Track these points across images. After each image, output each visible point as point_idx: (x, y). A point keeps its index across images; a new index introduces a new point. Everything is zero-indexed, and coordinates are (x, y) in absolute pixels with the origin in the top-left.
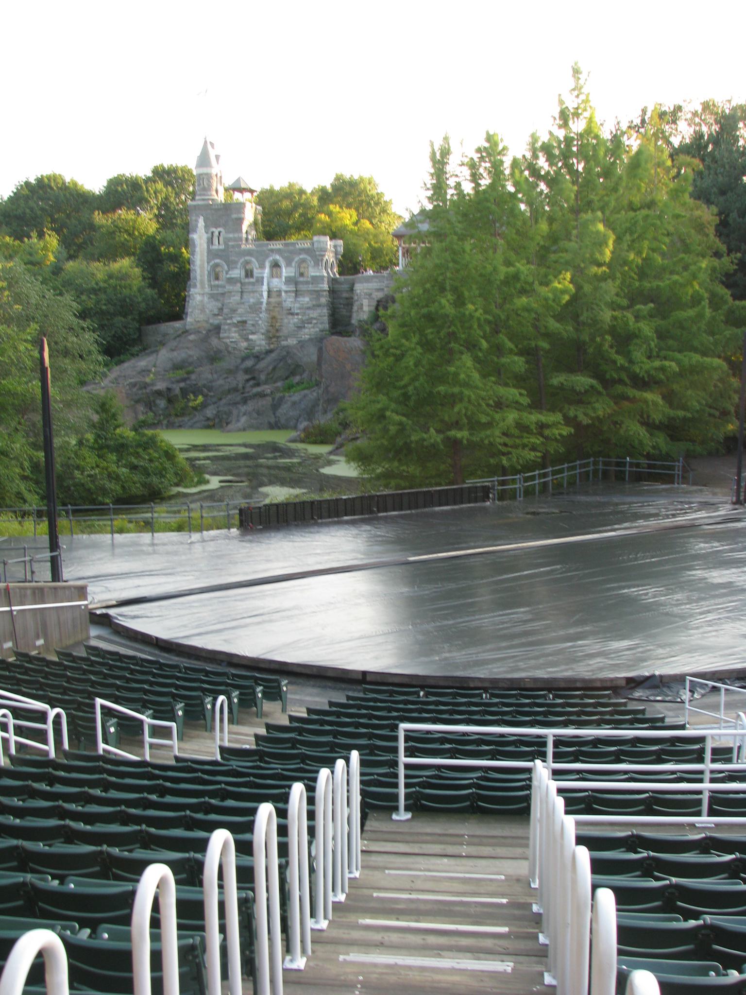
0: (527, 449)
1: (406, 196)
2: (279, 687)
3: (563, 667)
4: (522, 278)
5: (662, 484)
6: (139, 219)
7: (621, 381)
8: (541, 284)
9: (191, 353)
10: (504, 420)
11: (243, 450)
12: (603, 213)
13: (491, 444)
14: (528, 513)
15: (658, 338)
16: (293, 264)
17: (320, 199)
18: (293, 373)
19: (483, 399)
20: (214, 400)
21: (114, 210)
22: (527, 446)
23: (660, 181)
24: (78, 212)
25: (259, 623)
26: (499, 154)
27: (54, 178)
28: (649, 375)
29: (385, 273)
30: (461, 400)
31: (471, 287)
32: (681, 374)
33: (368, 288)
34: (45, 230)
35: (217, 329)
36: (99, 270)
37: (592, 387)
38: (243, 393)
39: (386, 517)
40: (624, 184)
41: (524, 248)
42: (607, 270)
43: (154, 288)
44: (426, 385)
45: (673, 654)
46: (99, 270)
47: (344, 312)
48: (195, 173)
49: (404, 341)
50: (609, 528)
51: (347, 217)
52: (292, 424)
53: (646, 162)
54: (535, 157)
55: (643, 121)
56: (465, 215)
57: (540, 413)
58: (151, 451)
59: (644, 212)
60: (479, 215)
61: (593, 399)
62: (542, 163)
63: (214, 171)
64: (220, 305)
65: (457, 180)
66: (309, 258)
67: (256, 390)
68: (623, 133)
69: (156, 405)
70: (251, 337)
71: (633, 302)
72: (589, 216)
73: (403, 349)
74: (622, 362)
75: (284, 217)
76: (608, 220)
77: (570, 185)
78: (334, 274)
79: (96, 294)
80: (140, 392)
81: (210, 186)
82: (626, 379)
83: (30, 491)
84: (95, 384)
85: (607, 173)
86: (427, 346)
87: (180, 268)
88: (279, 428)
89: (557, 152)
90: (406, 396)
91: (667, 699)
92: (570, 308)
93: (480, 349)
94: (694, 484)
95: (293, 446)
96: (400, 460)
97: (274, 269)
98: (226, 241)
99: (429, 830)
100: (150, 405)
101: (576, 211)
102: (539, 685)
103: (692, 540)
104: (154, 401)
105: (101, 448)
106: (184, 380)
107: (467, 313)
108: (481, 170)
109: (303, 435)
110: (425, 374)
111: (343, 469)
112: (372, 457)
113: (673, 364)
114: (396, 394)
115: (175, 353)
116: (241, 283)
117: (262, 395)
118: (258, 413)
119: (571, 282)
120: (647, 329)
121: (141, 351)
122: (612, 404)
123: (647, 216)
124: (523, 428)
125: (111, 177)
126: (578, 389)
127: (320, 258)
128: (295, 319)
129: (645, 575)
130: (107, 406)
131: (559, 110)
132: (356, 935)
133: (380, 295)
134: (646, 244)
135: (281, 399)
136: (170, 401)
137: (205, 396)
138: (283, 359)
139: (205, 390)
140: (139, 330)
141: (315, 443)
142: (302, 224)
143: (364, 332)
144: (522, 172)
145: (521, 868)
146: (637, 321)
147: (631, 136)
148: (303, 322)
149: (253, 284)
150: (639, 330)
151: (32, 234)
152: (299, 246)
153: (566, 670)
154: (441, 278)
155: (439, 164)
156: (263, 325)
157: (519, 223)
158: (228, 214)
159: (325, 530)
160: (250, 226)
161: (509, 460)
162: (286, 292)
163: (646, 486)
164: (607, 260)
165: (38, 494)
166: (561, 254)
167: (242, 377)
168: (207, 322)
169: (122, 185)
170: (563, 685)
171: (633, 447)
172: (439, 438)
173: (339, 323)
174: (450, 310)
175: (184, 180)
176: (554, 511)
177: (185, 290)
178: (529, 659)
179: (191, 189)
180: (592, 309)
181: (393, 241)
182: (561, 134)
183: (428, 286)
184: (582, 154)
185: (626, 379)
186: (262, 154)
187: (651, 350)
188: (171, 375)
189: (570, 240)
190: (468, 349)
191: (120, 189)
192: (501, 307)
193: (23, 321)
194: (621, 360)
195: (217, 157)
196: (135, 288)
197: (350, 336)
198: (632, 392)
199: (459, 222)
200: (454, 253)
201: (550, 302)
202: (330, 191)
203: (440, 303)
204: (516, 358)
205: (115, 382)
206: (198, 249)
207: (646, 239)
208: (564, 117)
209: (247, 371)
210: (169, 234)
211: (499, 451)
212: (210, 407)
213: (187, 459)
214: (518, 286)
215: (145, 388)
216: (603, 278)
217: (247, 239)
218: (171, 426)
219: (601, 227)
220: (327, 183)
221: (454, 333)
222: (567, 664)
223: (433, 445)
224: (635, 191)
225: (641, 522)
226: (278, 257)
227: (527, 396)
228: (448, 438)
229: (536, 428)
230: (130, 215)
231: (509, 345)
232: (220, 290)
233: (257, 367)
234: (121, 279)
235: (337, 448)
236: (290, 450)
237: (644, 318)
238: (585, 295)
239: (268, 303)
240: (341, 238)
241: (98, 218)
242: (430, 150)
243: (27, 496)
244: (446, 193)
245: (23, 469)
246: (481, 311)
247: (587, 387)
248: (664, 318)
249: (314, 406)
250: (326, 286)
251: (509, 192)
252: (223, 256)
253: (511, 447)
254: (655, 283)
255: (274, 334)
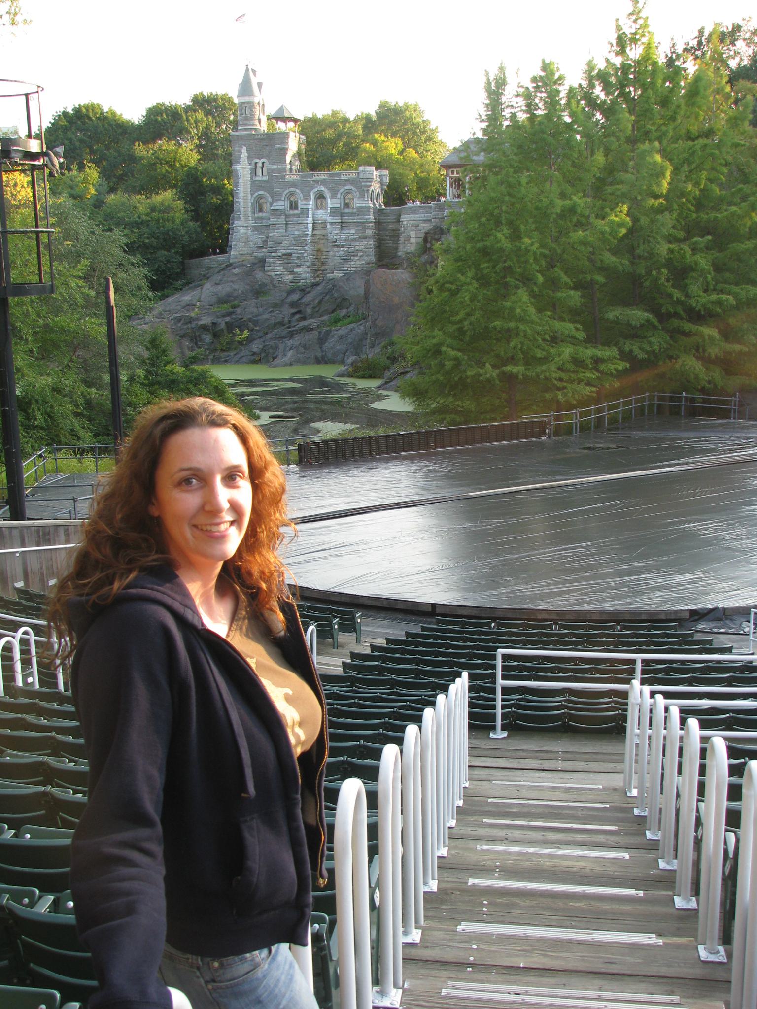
0: (583, 384)
1: (456, 124)
2: (354, 619)
3: (628, 600)
4: (579, 211)
5: (718, 419)
6: (180, 151)
7: (676, 315)
8: (597, 217)
9: (236, 286)
10: (560, 355)
11: (290, 385)
12: (660, 143)
13: (546, 379)
14: (584, 449)
15: (714, 270)
16: (339, 196)
17: (365, 127)
18: (339, 307)
19: (538, 333)
20: (260, 334)
21: (154, 140)
22: (582, 381)
23: (718, 109)
24: (117, 143)
25: (328, 557)
26: (555, 83)
27: (91, 108)
28: (705, 309)
29: (433, 204)
30: (517, 335)
31: (527, 221)
32: (737, 308)
33: (414, 221)
34: (85, 162)
35: (262, 262)
36: (141, 203)
37: (648, 321)
38: (289, 327)
39: (443, 452)
40: (682, 113)
41: (580, 180)
42: (665, 202)
43: (196, 221)
44: (482, 320)
45: (735, 587)
46: (141, 203)
47: (390, 244)
48: (236, 101)
49: (459, 275)
50: (667, 463)
51: (392, 146)
52: (339, 357)
53: (705, 90)
54: (592, 86)
55: (700, 43)
56: (520, 147)
57: (595, 348)
58: (202, 387)
59: (702, 141)
60: (534, 146)
61: (650, 334)
62: (598, 91)
63: (256, 100)
64: (263, 237)
65: (513, 111)
66: (354, 189)
67: (305, 323)
68: (678, 56)
69: (201, 340)
70: (295, 270)
71: (689, 235)
72: (646, 146)
73: (458, 284)
74: (679, 295)
75: (329, 146)
76: (664, 150)
77: (627, 115)
78: (380, 205)
79: (139, 228)
80: (185, 327)
81: (253, 115)
82: (682, 313)
83: (83, 428)
84: (140, 319)
85: (665, 102)
86: (483, 281)
87: (223, 200)
88: (326, 363)
89: (613, 80)
90: (461, 331)
91: (730, 631)
92: (626, 241)
93: (535, 284)
94: (750, 419)
95: (342, 380)
96: (455, 395)
97: (319, 201)
98: (271, 172)
99: (525, 747)
100: (196, 340)
101: (633, 141)
102: (604, 617)
103: (750, 475)
104: (199, 336)
105: (151, 384)
106: (229, 314)
107: (523, 247)
108: (537, 101)
109: (350, 370)
110: (482, 309)
111: (394, 403)
112: (427, 392)
113: (731, 298)
114: (451, 329)
115: (220, 287)
116: (286, 215)
117: (309, 329)
118: (305, 347)
119: (627, 215)
120: (703, 262)
121: (184, 285)
122: (668, 338)
123: (706, 145)
124: (578, 362)
125: (150, 106)
126: (633, 323)
127: (366, 189)
128: (341, 252)
129: (704, 510)
130: (157, 343)
131: (616, 36)
132: (482, 831)
133: (427, 227)
134: (704, 174)
135: (328, 333)
136: (215, 335)
137: (251, 330)
138: (329, 292)
139: (251, 325)
140: (182, 263)
141: (363, 377)
142: (347, 154)
143: (412, 265)
144: (578, 102)
145: (617, 781)
146: (694, 254)
147: (687, 58)
148: (349, 254)
149: (298, 216)
150: (696, 263)
151: (72, 167)
152: (344, 177)
153: (631, 603)
154: (496, 212)
155: (495, 91)
156: (308, 258)
157: (576, 155)
158: (271, 144)
159: (384, 465)
160: (293, 156)
161: (565, 395)
162: (331, 223)
163: (702, 421)
164: (664, 192)
165: (92, 431)
166: (617, 186)
167: (287, 311)
168: (251, 255)
169: (162, 115)
170: (628, 617)
171: (688, 382)
172: (495, 373)
173: (385, 255)
174: (506, 244)
175: (224, 109)
176: (611, 446)
177: (228, 223)
178: (595, 592)
179: (232, 118)
180: (649, 242)
181: (439, 170)
182: (618, 61)
183: (483, 220)
184: (636, 82)
185: (682, 313)
186: (306, 80)
187: (708, 283)
188: (216, 309)
189: (627, 172)
190: (524, 283)
191: (159, 119)
192: (556, 240)
193: (75, 257)
194: (677, 294)
195: (260, 85)
196: (178, 221)
197: (396, 269)
198: (688, 326)
199: (515, 154)
200: (510, 186)
201: (606, 235)
202: (374, 118)
203: (496, 237)
204: (572, 292)
205: (161, 316)
206: (241, 181)
207: (704, 169)
208: (622, 43)
209: (293, 305)
210: (210, 166)
211: (554, 385)
212: (256, 342)
213: (236, 394)
214: (575, 220)
215: (190, 322)
216: (660, 210)
217: (291, 169)
218: (217, 361)
219: (658, 158)
220: (371, 109)
221: (510, 267)
222: (630, 597)
223: (488, 381)
224: (693, 120)
225: (699, 458)
226: (323, 188)
227: (583, 330)
228: (504, 373)
229: (591, 363)
230: (171, 146)
231: (565, 279)
232: (265, 223)
233: (303, 301)
234: (164, 212)
235: (386, 383)
236: (338, 384)
237: (701, 251)
238: (641, 228)
239: (313, 236)
240: (387, 168)
241: (139, 149)
242: (485, 79)
243: (82, 433)
244: (501, 125)
245: (77, 406)
246: (537, 245)
247: (642, 322)
248: (720, 250)
249: (361, 340)
250: (372, 218)
251: (566, 123)
252: (265, 188)
253: (567, 382)
254: (713, 215)
255: (319, 267)
